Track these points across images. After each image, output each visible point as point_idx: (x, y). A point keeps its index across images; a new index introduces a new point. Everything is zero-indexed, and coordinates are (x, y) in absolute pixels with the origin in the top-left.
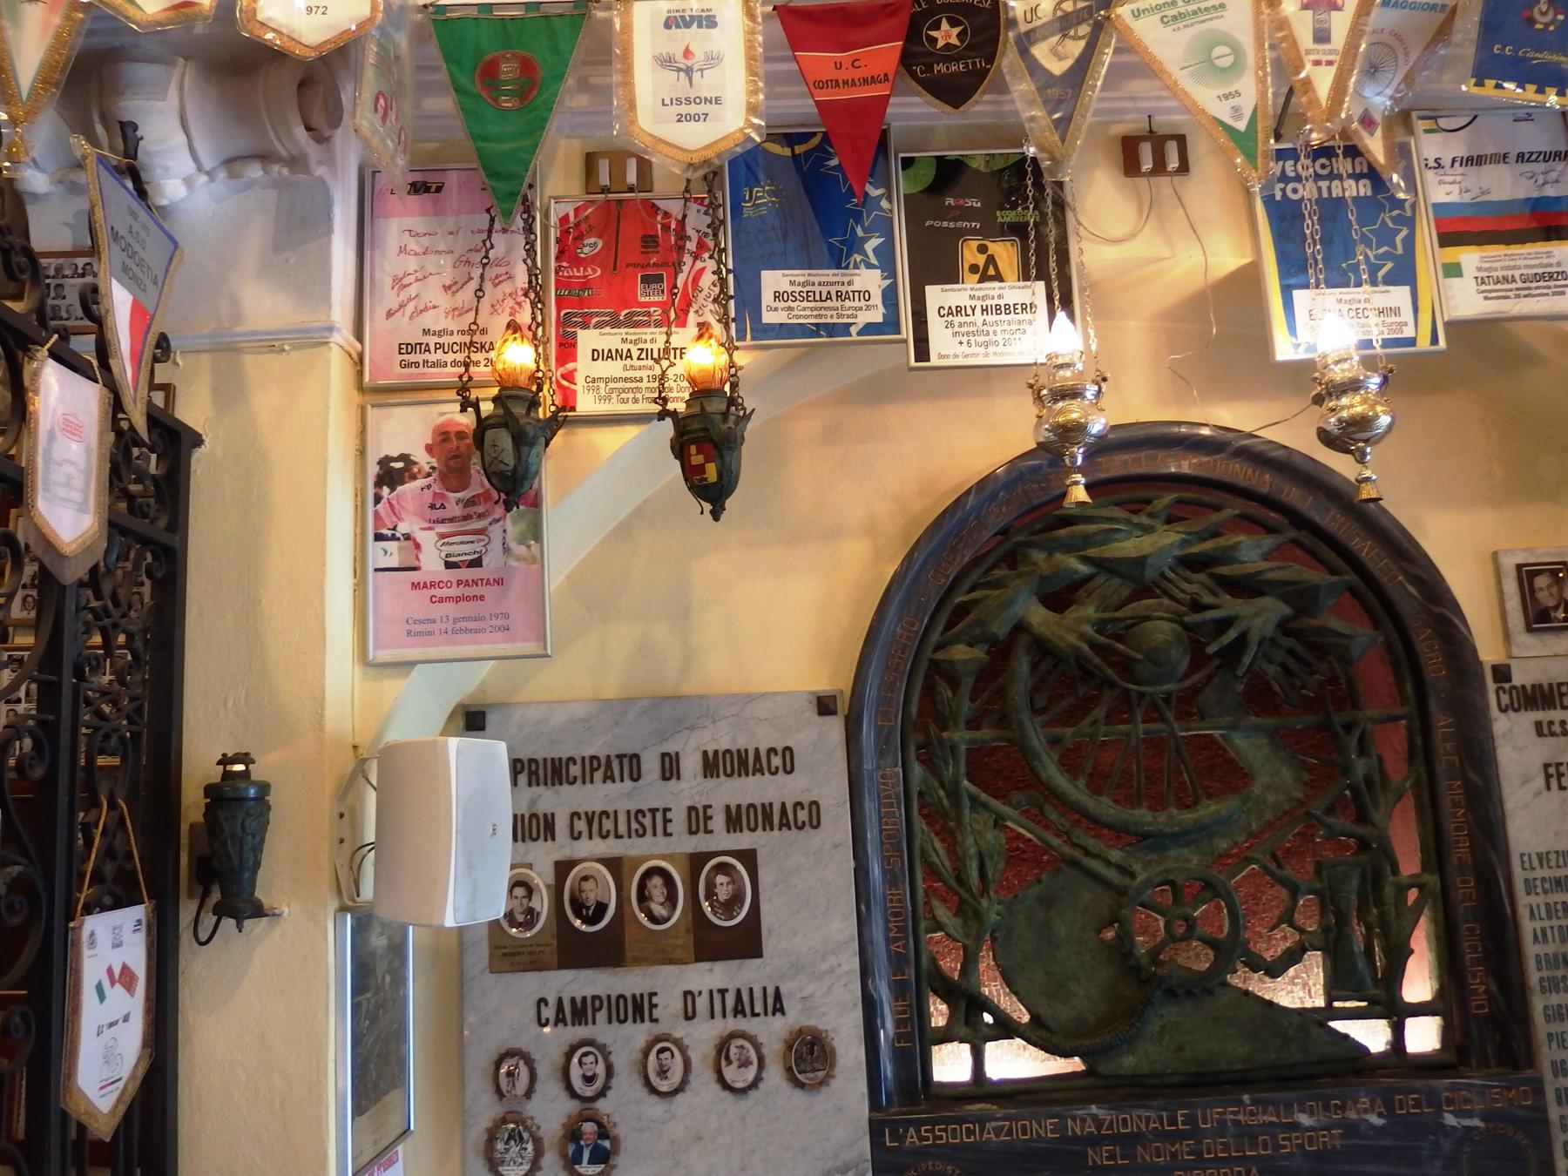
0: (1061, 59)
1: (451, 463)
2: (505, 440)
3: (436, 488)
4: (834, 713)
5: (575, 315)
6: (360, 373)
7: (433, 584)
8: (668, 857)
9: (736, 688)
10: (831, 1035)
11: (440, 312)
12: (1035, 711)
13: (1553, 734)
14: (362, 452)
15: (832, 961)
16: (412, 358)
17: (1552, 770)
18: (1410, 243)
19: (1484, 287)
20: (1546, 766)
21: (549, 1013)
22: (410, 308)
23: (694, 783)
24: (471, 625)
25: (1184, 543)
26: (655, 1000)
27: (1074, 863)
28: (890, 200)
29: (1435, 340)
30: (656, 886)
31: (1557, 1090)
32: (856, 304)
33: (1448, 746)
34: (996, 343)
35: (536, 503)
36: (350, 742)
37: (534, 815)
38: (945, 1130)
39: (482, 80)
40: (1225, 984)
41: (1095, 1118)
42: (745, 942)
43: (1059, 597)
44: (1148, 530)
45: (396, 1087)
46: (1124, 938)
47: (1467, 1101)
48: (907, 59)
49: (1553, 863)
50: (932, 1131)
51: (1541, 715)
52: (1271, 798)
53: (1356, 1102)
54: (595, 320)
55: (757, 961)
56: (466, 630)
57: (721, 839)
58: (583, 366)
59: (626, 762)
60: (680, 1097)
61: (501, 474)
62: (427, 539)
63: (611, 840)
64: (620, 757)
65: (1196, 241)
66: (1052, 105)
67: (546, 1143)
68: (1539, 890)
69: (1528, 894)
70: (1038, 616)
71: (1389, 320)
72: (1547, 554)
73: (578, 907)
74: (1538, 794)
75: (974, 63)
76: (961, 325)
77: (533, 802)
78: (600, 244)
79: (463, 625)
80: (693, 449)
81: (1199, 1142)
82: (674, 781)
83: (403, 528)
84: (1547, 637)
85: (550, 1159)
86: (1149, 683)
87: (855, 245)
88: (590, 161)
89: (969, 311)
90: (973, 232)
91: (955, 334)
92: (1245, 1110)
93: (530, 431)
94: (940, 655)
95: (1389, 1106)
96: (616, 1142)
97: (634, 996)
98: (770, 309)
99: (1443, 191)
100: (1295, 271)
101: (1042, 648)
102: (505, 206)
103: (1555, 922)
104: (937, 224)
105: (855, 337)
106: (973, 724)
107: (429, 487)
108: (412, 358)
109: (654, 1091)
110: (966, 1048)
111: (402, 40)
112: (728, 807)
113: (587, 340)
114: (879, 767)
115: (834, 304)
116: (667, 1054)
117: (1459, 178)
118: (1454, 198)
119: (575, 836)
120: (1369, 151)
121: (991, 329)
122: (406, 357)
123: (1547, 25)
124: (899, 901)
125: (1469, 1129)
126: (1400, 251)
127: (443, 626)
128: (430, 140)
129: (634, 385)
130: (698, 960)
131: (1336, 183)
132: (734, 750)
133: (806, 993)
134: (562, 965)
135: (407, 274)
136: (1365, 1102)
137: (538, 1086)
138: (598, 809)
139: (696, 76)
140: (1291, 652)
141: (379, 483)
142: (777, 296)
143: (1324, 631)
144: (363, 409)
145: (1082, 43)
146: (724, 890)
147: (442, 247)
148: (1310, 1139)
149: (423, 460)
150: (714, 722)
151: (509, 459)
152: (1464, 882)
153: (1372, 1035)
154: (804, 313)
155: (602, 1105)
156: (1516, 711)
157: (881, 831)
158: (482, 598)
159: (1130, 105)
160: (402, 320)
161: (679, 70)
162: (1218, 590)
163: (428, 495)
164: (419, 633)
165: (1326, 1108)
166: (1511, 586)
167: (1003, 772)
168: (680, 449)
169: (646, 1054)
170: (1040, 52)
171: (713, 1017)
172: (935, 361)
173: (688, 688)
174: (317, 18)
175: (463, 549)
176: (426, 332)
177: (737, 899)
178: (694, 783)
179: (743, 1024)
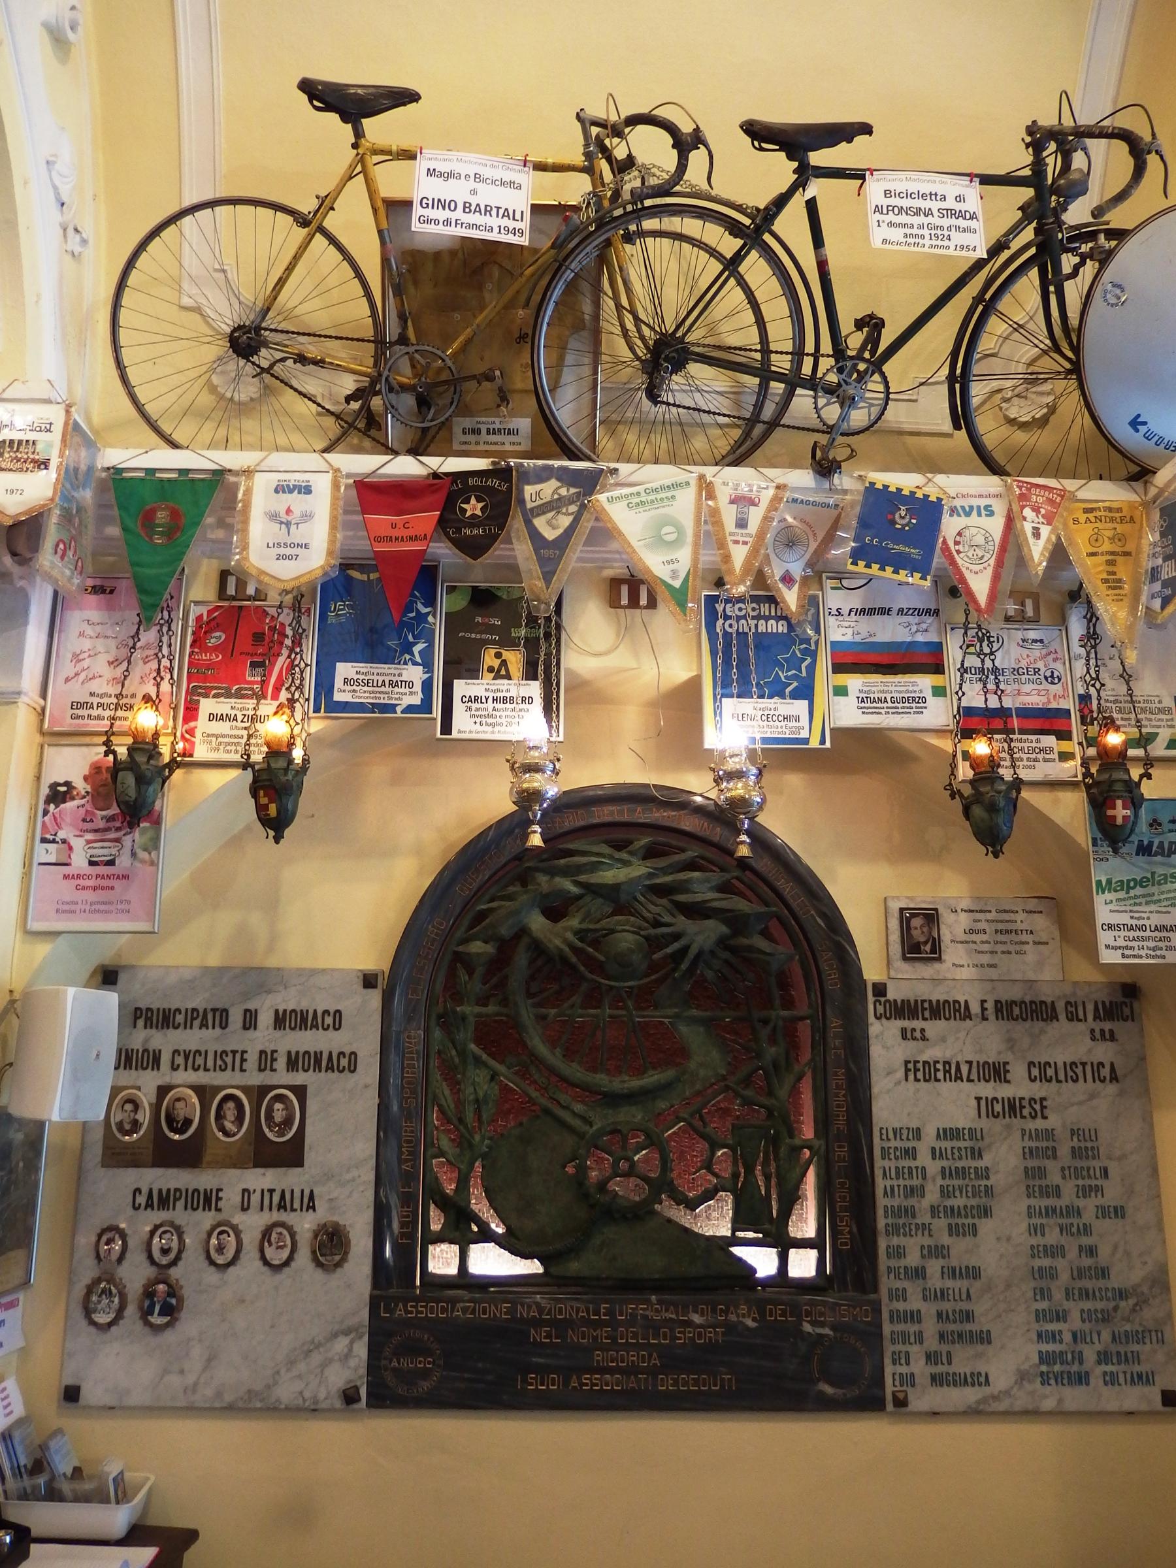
0: (554, 528)
1: (101, 789)
2: (129, 779)
3: (89, 807)
4: (375, 987)
5: (200, 687)
6: (42, 721)
7: (79, 876)
8: (245, 1089)
9: (307, 964)
10: (348, 1229)
11: (104, 681)
12: (530, 995)
13: (914, 1039)
14: (38, 778)
15: (355, 1173)
16: (80, 712)
17: (911, 1066)
18: (812, 669)
19: (863, 705)
20: (907, 1062)
21: (141, 1200)
22: (82, 676)
23: (266, 1033)
24: (102, 907)
25: (650, 876)
26: (221, 1194)
27: (547, 1112)
28: (435, 617)
29: (823, 742)
30: (230, 1109)
31: (891, 1311)
32: (403, 690)
33: (837, 1042)
34: (501, 724)
35: (157, 822)
36: (8, 987)
37: (146, 1051)
38: (425, 1307)
39: (143, 525)
40: (653, 1213)
41: (538, 1305)
42: (291, 1155)
43: (555, 911)
44: (626, 863)
45: (19, 1247)
46: (582, 1170)
47: (822, 1314)
48: (442, 523)
49: (904, 1137)
50: (416, 1307)
51: (906, 1023)
52: (702, 1072)
53: (737, 1307)
54: (214, 692)
55: (299, 1169)
56: (99, 911)
57: (282, 1076)
58: (202, 724)
59: (218, 1014)
60: (231, 1269)
61: (126, 803)
62: (78, 844)
63: (201, 1072)
64: (214, 1010)
65: (674, 655)
66: (542, 561)
67: (130, 1298)
68: (892, 1156)
69: (883, 1159)
70: (537, 922)
71: (790, 724)
72: (925, 902)
73: (170, 1119)
74: (898, 1083)
75: (490, 530)
76: (477, 710)
77: (146, 1040)
78: (223, 638)
79: (97, 907)
80: (262, 793)
81: (615, 1330)
82: (251, 1031)
83: (61, 835)
84: (918, 965)
85: (131, 1310)
86: (616, 979)
87: (408, 648)
88: (224, 575)
89: (484, 700)
90: (494, 642)
91: (471, 716)
92: (651, 1307)
93: (148, 774)
94: (461, 949)
95: (762, 1313)
96: (181, 1300)
97: (205, 1190)
98: (340, 690)
99: (839, 632)
100: (724, 687)
101: (538, 948)
102: (149, 614)
103: (901, 1182)
104: (468, 635)
105: (399, 715)
106: (483, 1001)
107: (83, 806)
108: (80, 712)
109: (212, 1263)
110: (455, 1248)
111: (87, 495)
112: (289, 1053)
113: (207, 706)
114: (406, 1029)
115: (387, 689)
116: (225, 1235)
117: (852, 624)
118: (848, 638)
119: (175, 1068)
120: (785, 602)
121: (498, 714)
122: (76, 712)
123: (904, 526)
124: (412, 1132)
125: (821, 1336)
126: (804, 674)
127: (83, 907)
128: (110, 555)
129: (236, 740)
130: (255, 1166)
131: (762, 622)
132: (298, 1010)
133: (334, 1195)
134: (155, 1164)
135: (82, 652)
136: (743, 1309)
137: (128, 1255)
138: (194, 1049)
139: (293, 528)
140: (726, 962)
141: (48, 801)
142: (346, 681)
143: (750, 949)
144: (42, 747)
145: (571, 518)
146: (279, 1116)
147: (109, 633)
148: (700, 1334)
149: (81, 786)
150: (286, 988)
151: (132, 793)
152: (840, 1147)
153: (762, 1261)
154: (364, 696)
155: (174, 1272)
156: (887, 1019)
157: (403, 1078)
158: (112, 888)
159: (617, 556)
160: (75, 685)
161: (282, 523)
162: (675, 912)
163: (82, 811)
164: (65, 912)
165: (714, 1311)
166: (894, 924)
167: (500, 1038)
168: (254, 792)
169: (210, 1235)
170: (540, 523)
171: (262, 1209)
172: (455, 734)
173: (272, 962)
174: (16, 498)
175: (102, 852)
176: (92, 694)
177: (288, 1122)
178: (266, 1033)
179: (284, 1216)
